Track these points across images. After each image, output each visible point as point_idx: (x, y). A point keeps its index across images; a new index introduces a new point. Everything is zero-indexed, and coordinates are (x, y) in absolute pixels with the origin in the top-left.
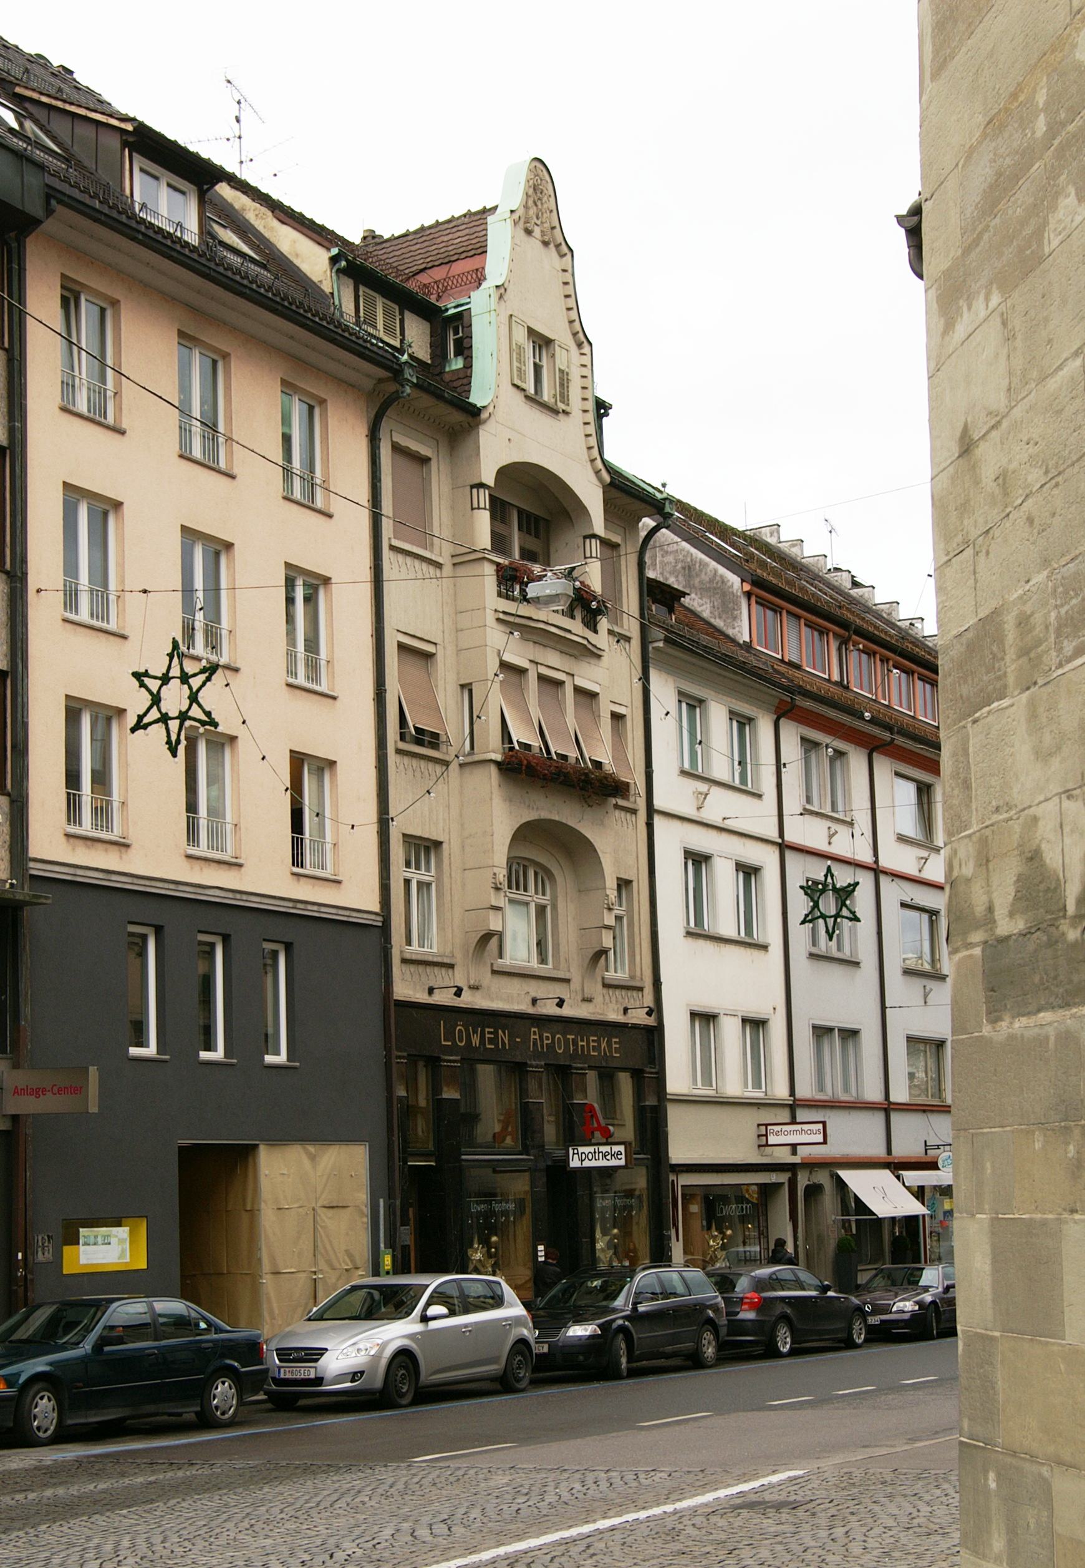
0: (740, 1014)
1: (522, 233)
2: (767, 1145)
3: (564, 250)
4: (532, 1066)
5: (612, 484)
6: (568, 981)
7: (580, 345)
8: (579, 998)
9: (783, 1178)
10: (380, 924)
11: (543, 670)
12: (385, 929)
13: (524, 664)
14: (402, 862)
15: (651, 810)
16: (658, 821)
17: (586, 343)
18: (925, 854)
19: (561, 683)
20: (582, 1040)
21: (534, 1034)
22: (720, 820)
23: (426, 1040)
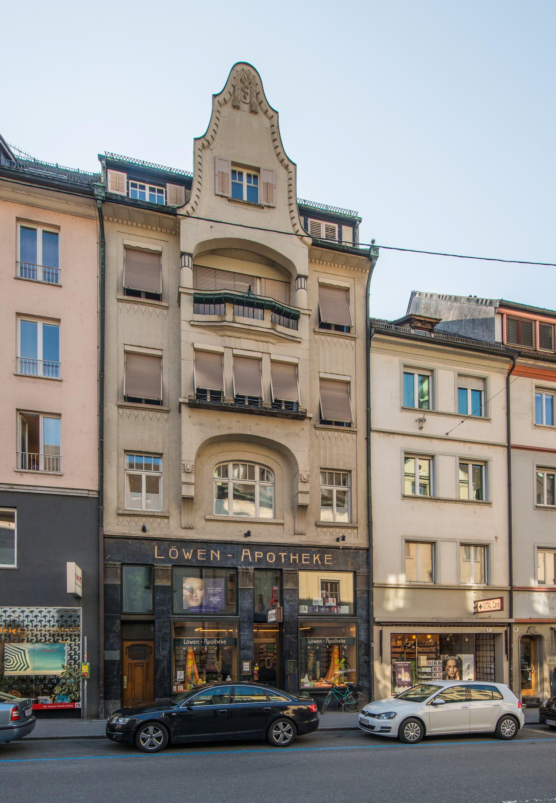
0: (458, 541)
1: (231, 109)
2: (477, 612)
3: (272, 115)
4: (157, 566)
5: (313, 244)
6: (282, 524)
7: (286, 167)
8: (293, 533)
9: (501, 630)
10: (97, 496)
11: (236, 352)
12: (99, 499)
13: (221, 350)
14: (532, 499)
15: (369, 430)
16: (373, 435)
17: (290, 164)
18: (421, 416)
19: (260, 360)
20: (295, 555)
21: (246, 552)
22: (445, 435)
23: (112, 554)
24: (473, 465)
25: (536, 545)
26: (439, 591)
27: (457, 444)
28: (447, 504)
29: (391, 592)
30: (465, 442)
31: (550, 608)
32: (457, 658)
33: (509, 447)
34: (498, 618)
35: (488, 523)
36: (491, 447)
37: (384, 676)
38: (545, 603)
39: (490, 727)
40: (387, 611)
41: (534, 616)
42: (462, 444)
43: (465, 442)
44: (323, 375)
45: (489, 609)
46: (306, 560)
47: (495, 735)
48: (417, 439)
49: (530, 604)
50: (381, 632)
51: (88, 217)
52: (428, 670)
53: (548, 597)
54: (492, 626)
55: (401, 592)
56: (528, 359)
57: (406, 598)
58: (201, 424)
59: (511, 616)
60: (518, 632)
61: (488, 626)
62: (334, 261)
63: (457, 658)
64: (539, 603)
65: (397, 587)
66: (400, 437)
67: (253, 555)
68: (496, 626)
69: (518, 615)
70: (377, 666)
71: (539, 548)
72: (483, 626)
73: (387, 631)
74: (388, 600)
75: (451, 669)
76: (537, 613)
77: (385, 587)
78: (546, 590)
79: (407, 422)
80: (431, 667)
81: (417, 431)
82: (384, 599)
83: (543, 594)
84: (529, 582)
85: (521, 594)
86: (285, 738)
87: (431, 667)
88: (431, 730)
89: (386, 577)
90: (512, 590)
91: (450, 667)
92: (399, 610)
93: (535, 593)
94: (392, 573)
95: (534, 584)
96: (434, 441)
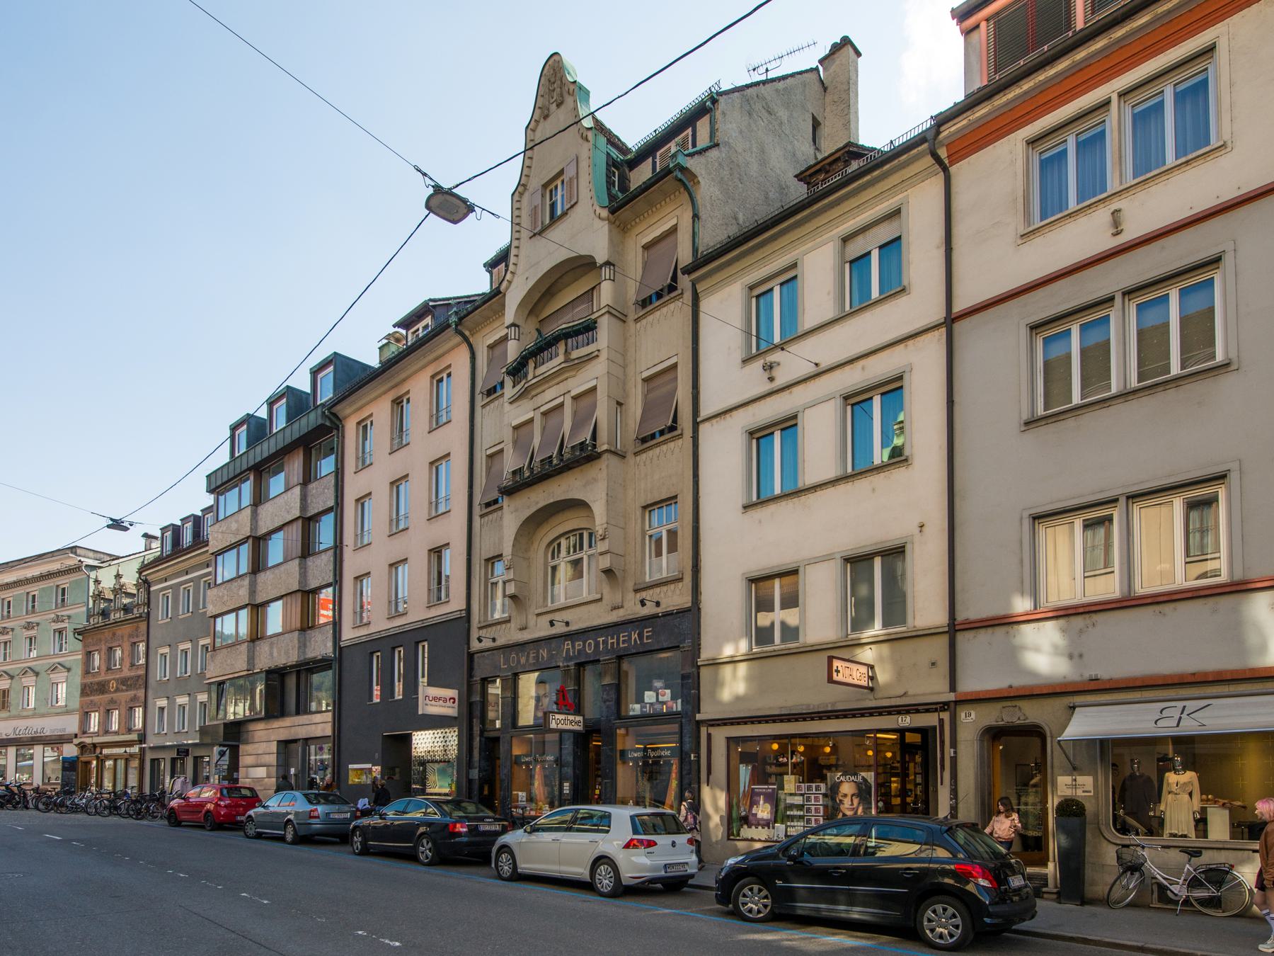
0: (838, 556)
24: (882, 394)
25: (1026, 514)
26: (803, 657)
27: (838, 373)
28: (819, 493)
29: (727, 670)
30: (851, 361)
31: (1071, 657)
32: (860, 779)
33: (951, 321)
34: (924, 695)
35: (902, 505)
36: (910, 343)
37: (717, 809)
38: (1055, 647)
39: (580, 871)
40: (720, 703)
41: (1018, 682)
42: (847, 368)
43: (851, 361)
44: (645, 375)
45: (850, 680)
46: (624, 642)
47: (586, 886)
48: (768, 399)
49: (1012, 655)
50: (709, 736)
51: (458, 345)
52: (798, 800)
53: (1063, 631)
54: (908, 712)
55: (742, 669)
56: (969, 113)
57: (750, 679)
58: (516, 510)
59: (953, 688)
60: (971, 721)
61: (899, 713)
62: (652, 205)
63: (860, 779)
64: (1037, 650)
65: (733, 661)
66: (741, 411)
67: (573, 646)
68: (918, 711)
69: (971, 683)
70: (706, 792)
71: (1037, 518)
72: (890, 713)
73: (720, 736)
74: (722, 684)
75: (847, 802)
76: (1034, 674)
77: (715, 664)
78: (1050, 614)
79: (753, 380)
80: (802, 795)
81: (768, 387)
82: (717, 683)
83: (1049, 625)
84: (1009, 603)
85: (983, 636)
86: (759, 912)
87: (802, 795)
88: (525, 866)
89: (720, 648)
90: (954, 629)
91: (845, 795)
92: (738, 699)
93: (1024, 627)
94: (727, 640)
95: (1022, 605)
96: (795, 390)
